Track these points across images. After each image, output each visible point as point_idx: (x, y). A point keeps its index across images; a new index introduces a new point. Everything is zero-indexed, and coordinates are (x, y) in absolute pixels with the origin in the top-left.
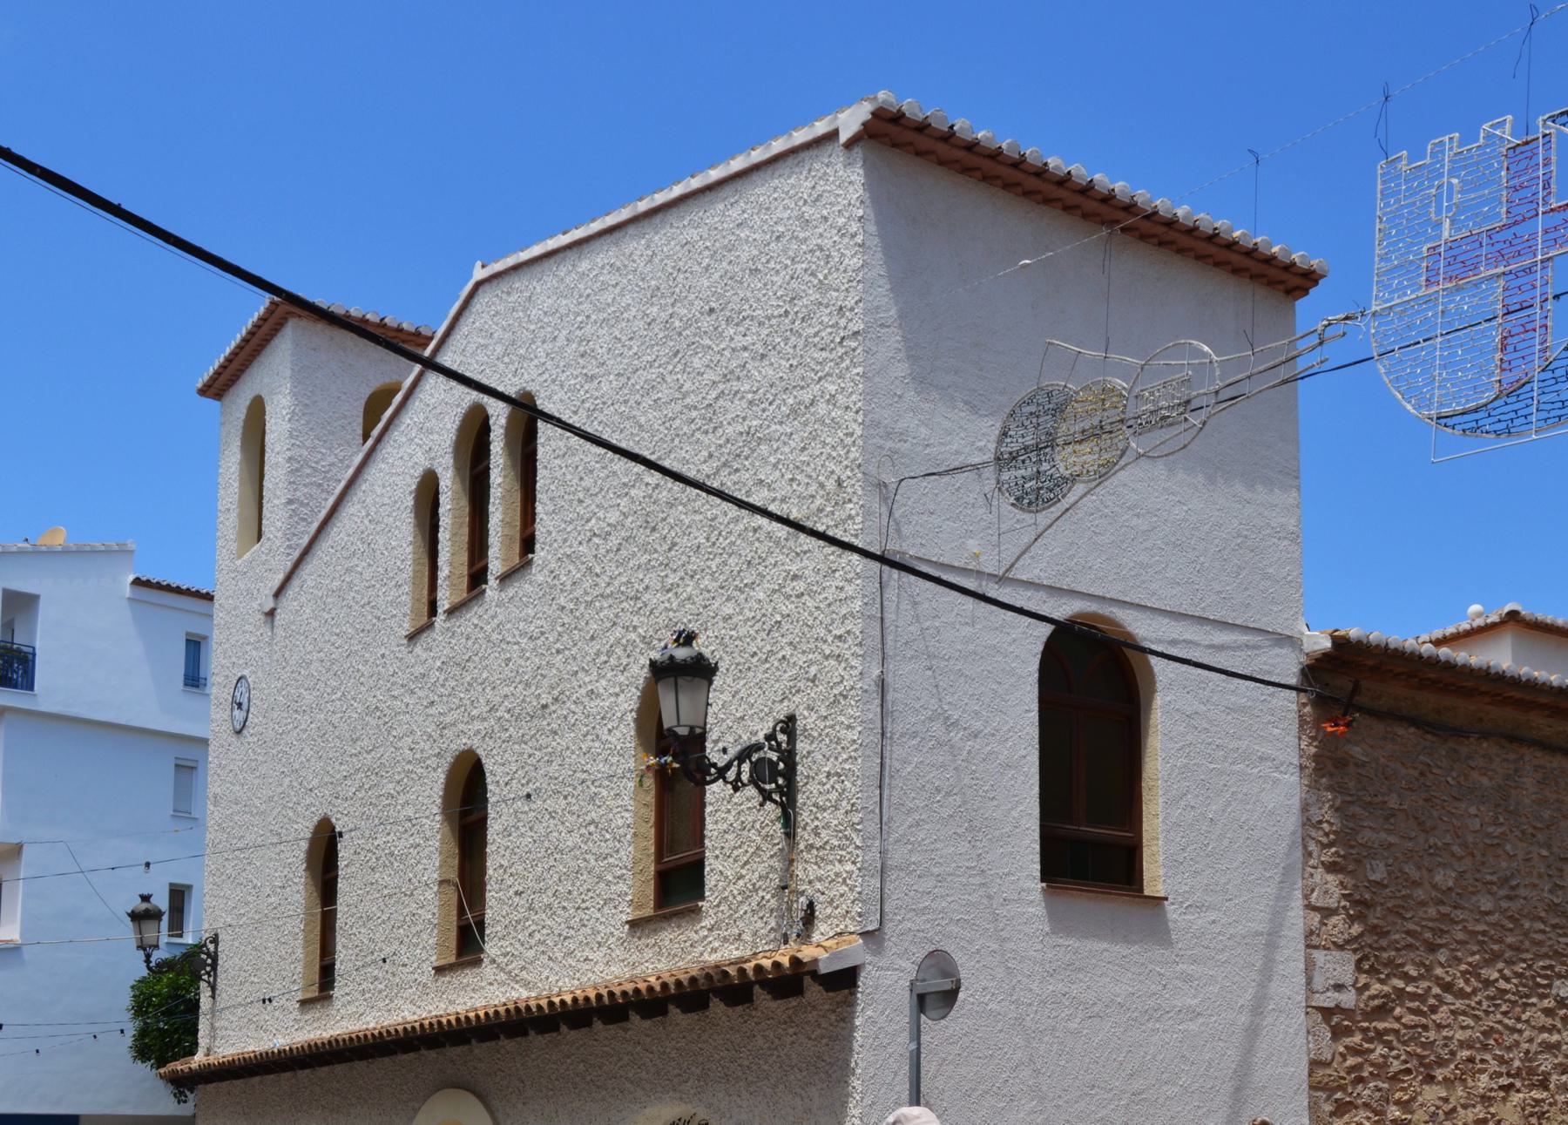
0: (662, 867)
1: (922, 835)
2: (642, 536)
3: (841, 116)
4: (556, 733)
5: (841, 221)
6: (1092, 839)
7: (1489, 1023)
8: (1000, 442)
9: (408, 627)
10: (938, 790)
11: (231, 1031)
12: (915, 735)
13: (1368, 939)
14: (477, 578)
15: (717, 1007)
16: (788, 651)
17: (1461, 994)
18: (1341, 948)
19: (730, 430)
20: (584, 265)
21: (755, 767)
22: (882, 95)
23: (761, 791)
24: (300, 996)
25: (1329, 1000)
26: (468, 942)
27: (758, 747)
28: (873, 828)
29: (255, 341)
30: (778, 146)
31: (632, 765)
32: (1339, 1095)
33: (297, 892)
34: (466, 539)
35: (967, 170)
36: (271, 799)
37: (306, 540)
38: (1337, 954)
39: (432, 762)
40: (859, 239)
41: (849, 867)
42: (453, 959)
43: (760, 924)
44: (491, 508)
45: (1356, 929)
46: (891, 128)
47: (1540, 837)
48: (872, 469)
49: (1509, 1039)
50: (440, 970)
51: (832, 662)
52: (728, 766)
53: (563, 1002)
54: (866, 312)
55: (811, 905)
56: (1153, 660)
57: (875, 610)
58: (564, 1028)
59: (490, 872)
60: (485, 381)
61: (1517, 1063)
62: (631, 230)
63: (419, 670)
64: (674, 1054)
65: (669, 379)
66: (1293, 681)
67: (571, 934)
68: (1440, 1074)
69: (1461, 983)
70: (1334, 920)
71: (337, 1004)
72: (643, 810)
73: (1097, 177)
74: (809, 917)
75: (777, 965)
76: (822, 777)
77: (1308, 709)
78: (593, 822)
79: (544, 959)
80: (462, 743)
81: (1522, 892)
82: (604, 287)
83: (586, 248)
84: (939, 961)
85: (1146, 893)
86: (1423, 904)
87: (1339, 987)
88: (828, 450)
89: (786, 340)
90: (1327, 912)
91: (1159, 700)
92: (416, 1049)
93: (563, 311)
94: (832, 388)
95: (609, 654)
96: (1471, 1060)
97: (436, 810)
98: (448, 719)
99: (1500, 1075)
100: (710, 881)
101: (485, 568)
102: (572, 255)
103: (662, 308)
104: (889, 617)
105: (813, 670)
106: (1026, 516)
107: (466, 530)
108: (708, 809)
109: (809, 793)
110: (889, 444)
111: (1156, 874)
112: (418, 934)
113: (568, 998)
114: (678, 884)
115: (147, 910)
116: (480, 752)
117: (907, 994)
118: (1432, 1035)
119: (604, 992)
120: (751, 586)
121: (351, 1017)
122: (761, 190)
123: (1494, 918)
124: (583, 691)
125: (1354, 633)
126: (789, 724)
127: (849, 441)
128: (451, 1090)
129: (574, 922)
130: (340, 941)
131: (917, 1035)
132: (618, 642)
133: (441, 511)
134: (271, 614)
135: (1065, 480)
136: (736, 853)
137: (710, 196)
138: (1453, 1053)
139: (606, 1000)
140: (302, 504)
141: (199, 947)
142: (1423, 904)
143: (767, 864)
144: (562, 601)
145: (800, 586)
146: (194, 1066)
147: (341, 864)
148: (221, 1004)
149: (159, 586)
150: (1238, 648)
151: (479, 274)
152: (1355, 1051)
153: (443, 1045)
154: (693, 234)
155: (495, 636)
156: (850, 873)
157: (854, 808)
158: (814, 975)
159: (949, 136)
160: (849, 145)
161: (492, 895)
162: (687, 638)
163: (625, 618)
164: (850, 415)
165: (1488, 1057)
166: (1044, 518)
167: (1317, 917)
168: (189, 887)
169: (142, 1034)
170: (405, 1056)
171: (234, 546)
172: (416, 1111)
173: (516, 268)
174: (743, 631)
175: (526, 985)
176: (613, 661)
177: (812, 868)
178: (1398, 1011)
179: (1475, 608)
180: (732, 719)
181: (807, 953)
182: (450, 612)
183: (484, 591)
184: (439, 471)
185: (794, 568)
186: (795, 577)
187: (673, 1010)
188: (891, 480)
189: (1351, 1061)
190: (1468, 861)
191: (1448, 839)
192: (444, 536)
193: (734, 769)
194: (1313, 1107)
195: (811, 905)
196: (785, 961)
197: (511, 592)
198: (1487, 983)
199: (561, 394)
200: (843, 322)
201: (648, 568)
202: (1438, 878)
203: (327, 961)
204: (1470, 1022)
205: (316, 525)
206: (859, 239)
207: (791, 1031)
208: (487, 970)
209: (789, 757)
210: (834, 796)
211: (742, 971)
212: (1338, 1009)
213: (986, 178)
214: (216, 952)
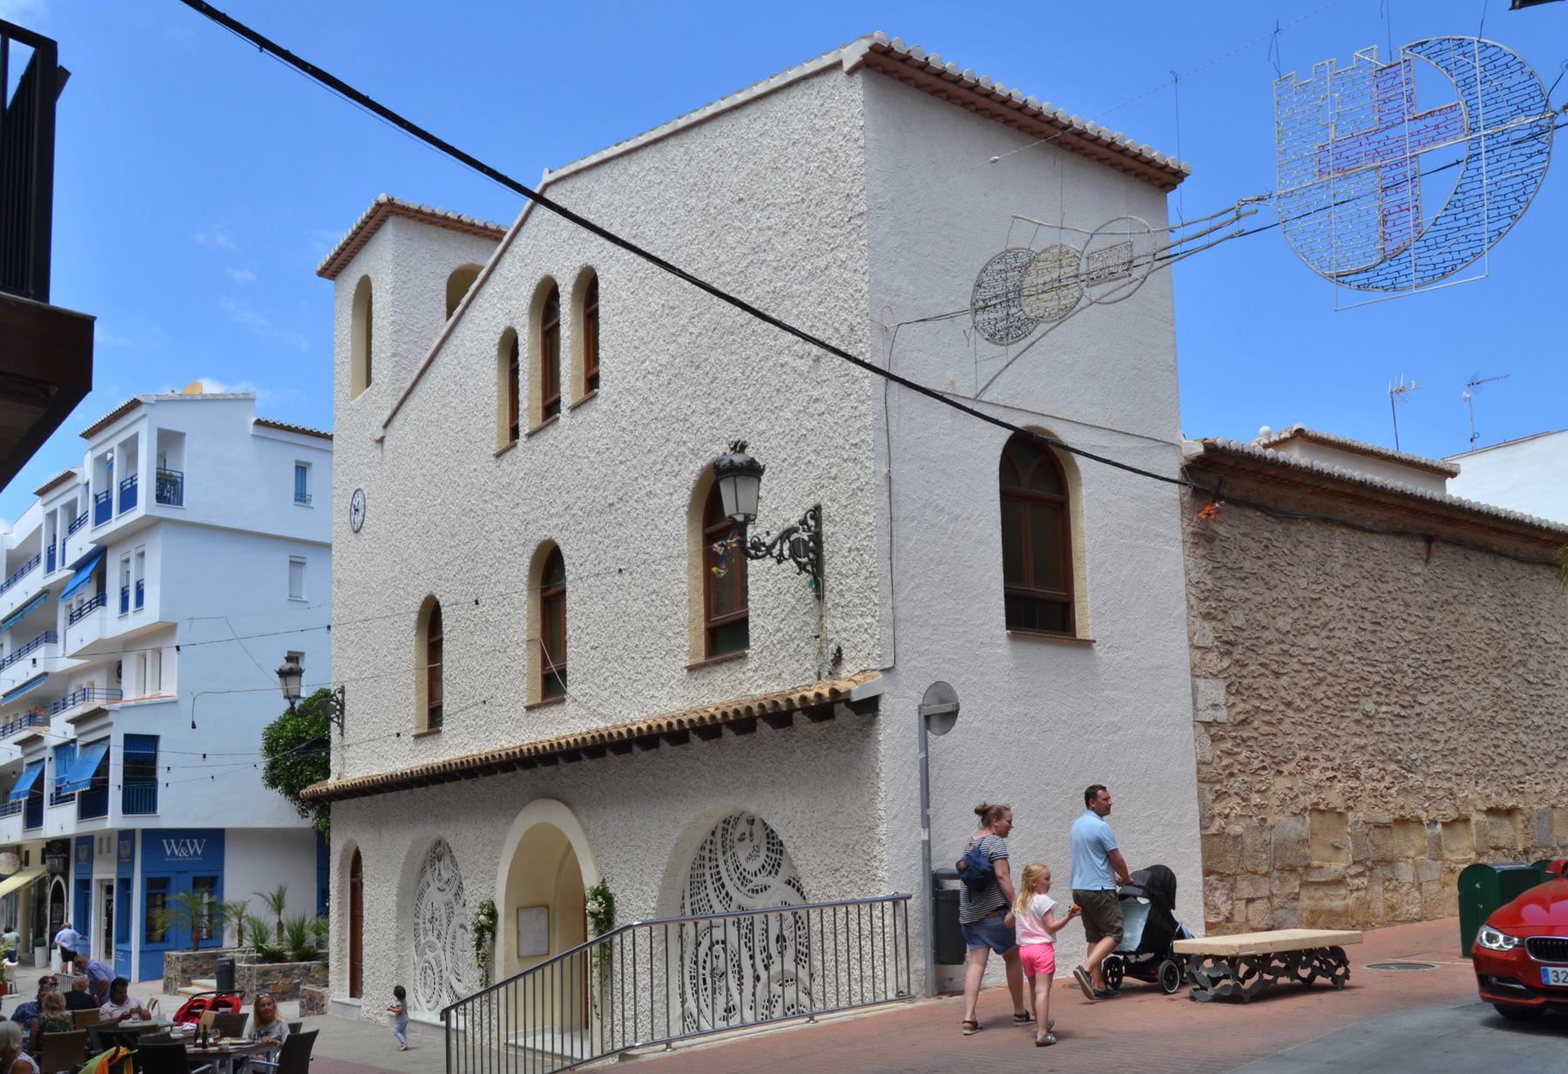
1: (921, 595)
2: (688, 372)
3: (844, 51)
5: (846, 129)
6: (1040, 601)
7: (1318, 730)
8: (975, 291)
10: (931, 560)
11: (356, 759)
12: (913, 519)
13: (1234, 670)
14: (551, 409)
16: (813, 457)
17: (1299, 710)
19: (758, 290)
21: (793, 544)
22: (877, 34)
23: (799, 563)
24: (415, 732)
25: (1207, 716)
26: (552, 686)
27: (794, 530)
28: (887, 590)
29: (363, 233)
30: (792, 75)
31: (685, 547)
32: (1218, 787)
33: (410, 651)
34: (540, 379)
35: (935, 92)
36: (385, 582)
37: (408, 385)
38: (1213, 682)
39: (519, 550)
40: (861, 143)
41: (869, 620)
43: (796, 665)
44: (562, 355)
45: (1226, 662)
46: (883, 59)
48: (877, 317)
49: (1333, 742)
50: (530, 708)
51: (850, 464)
52: (773, 545)
53: (639, 729)
54: (868, 198)
55: (839, 650)
57: (882, 424)
58: (561, 762)
59: (569, 632)
61: (1338, 761)
62: (672, 141)
63: (505, 480)
65: (707, 253)
66: (1176, 477)
68: (1286, 768)
70: (1211, 656)
71: (445, 737)
73: (1030, 98)
74: (838, 658)
75: (818, 695)
76: (845, 552)
77: (1186, 499)
78: (654, 592)
79: (617, 697)
80: (543, 535)
81: (1337, 633)
82: (651, 184)
83: (635, 156)
84: (941, 691)
85: (1079, 636)
86: (1270, 643)
87: (1215, 706)
88: (841, 303)
89: (804, 220)
90: (1207, 650)
92: (442, 782)
93: (617, 204)
94: (843, 256)
95: (664, 463)
96: (1306, 759)
97: (523, 587)
99: (1326, 769)
100: (754, 633)
101: (558, 401)
102: (624, 162)
103: (700, 199)
104: (893, 429)
105: (834, 471)
106: (998, 348)
107: (540, 373)
108: (750, 579)
109: (834, 564)
110: (888, 298)
111: (1087, 620)
112: (511, 682)
113: (644, 727)
114: (726, 635)
116: (559, 541)
117: (916, 716)
118: (1280, 740)
119: (674, 721)
120: (780, 408)
121: (459, 744)
122: (777, 105)
123: (1317, 653)
124: (643, 492)
125: (1220, 442)
127: (858, 295)
128: (540, 801)
129: (642, 668)
130: (447, 689)
131: (925, 746)
132: (671, 453)
133: (520, 358)
134: (381, 441)
135: (1031, 321)
137: (736, 114)
138: (1294, 754)
139: (675, 726)
141: (324, 696)
142: (1270, 643)
144: (623, 424)
145: (821, 407)
146: (331, 787)
147: (445, 630)
149: (275, 426)
152: (1229, 754)
153: (476, 776)
154: (723, 142)
155: (568, 453)
156: (870, 624)
157: (871, 575)
158: (848, 702)
159: (924, 66)
160: (851, 72)
161: (572, 650)
162: (740, 447)
163: (676, 436)
164: (858, 276)
165: (1318, 756)
166: (1014, 349)
167: (1198, 654)
169: (272, 766)
170: (504, 775)
171: (348, 391)
172: (514, 817)
173: (577, 173)
174: (775, 443)
176: (667, 469)
177: (839, 623)
178: (1256, 724)
179: (1264, 429)
180: (773, 509)
181: (842, 686)
182: (530, 435)
184: (517, 328)
185: (815, 394)
186: (817, 400)
187: (636, 749)
188: (891, 325)
189: (1225, 762)
190: (1300, 610)
191: (1285, 594)
192: (523, 377)
194: (1201, 796)
195: (839, 650)
196: (826, 692)
197: (580, 418)
198: (1315, 701)
199: (618, 267)
200: (850, 206)
201: (694, 397)
203: (435, 704)
204: (1304, 730)
205: (417, 372)
206: (861, 143)
208: (569, 706)
209: (817, 537)
210: (855, 566)
211: (790, 701)
212: (1215, 723)
213: (950, 99)
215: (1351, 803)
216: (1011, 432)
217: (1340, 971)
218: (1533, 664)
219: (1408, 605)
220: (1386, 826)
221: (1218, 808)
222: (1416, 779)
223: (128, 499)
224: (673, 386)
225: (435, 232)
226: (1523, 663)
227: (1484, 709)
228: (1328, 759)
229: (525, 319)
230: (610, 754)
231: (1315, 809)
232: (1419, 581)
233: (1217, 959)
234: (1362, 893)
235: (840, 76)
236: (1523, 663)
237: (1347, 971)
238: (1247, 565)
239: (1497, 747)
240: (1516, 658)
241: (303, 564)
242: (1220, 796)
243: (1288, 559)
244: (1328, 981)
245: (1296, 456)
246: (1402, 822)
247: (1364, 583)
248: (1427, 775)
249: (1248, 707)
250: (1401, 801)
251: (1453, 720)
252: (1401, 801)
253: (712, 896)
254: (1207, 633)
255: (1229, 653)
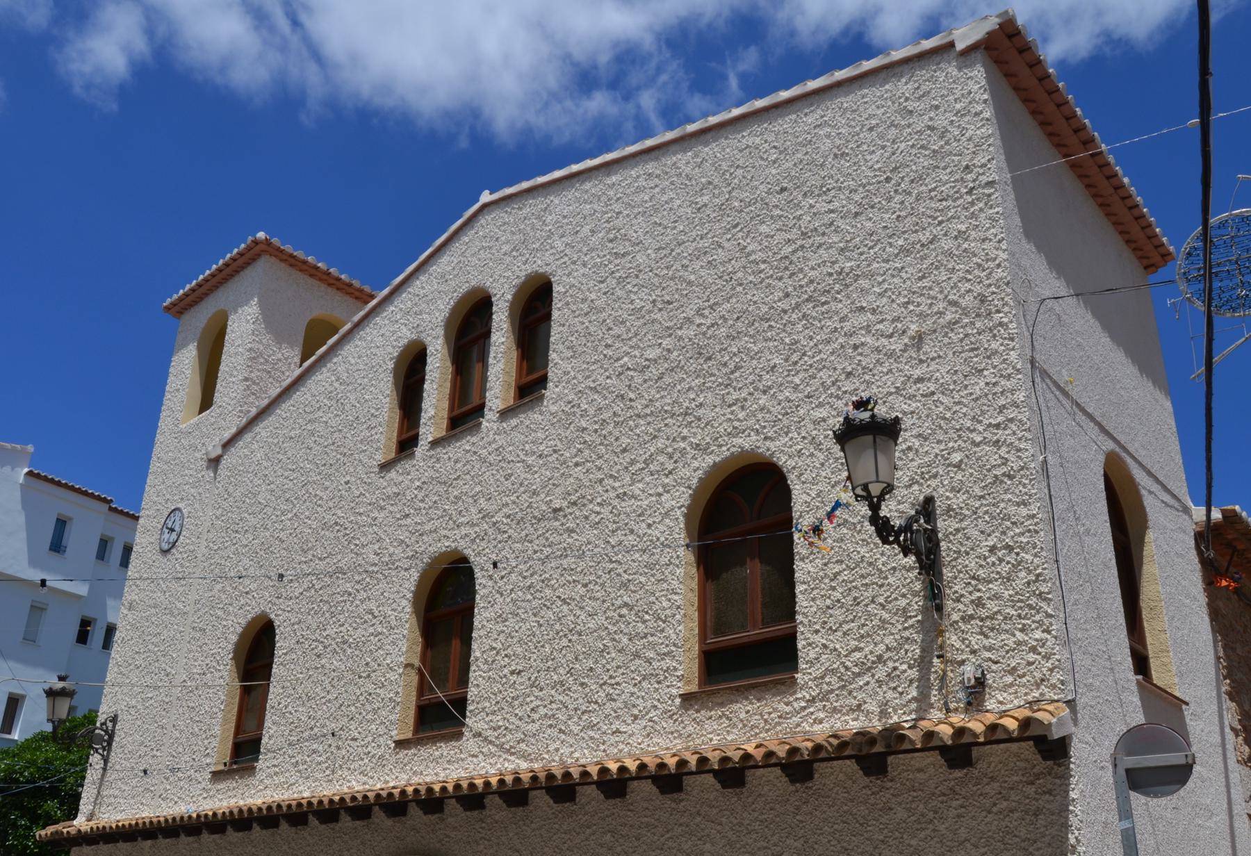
0: (706, 648)
4: (573, 531)
9: (380, 457)
14: (465, 415)
15: (345, 820)
20: (614, 179)
24: (213, 769)
33: (223, 679)
42: (409, 735)
50: (400, 744)
64: (756, 826)
71: (260, 775)
72: (690, 595)
79: (555, 732)
91: (1150, 536)
98: (427, 527)
108: (799, 588)
115: (63, 689)
131: (1125, 812)
134: (215, 462)
136: (846, 627)
140: (254, 383)
143: (899, 635)
148: (111, 776)
150: (1171, 507)
151: (486, 197)
156: (1043, 643)
168: (23, 697)
175: (525, 756)
183: (480, 424)
184: (428, 340)
187: (229, 829)
201: (702, 389)
207: (955, 804)
208: (469, 742)
214: (113, 731)
224: (667, 379)
225: (302, 278)
230: (284, 826)
241: (43, 609)
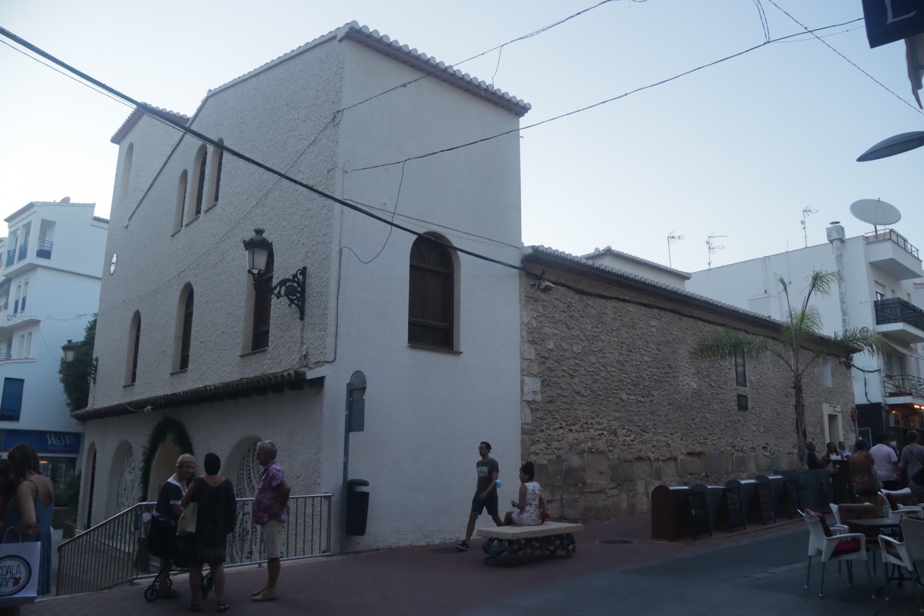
11: (99, 399)
17: (583, 396)
18: (535, 376)
27: (288, 280)
45: (543, 368)
47: (614, 333)
56: (459, 253)
60: (241, 153)
67: (220, 360)
69: (583, 392)
80: (186, 281)
100: (271, 338)
114: (259, 340)
121: (141, 392)
123: (595, 366)
126: (304, 271)
134: (127, 227)
160: (340, 41)
162: (259, 232)
167: (526, 363)
178: (558, 403)
182: (187, 226)
193: (278, 289)
198: (593, 392)
202: (575, 349)
204: (587, 408)
209: (303, 286)
215: (611, 448)
216: (416, 236)
217: (571, 547)
218: (714, 377)
219: (647, 342)
220: (630, 461)
221: (533, 448)
222: (647, 436)
223: (23, 255)
226: (709, 376)
227: (687, 399)
228: (599, 424)
229: (192, 165)
231: (590, 451)
232: (654, 330)
233: (500, 541)
234: (615, 498)
235: (336, 42)
236: (709, 376)
237: (574, 547)
238: (557, 316)
239: (693, 419)
240: (705, 373)
242: (534, 443)
243: (581, 313)
244: (564, 553)
245: (608, 264)
246: (640, 459)
247: (623, 329)
248: (656, 434)
249: (554, 394)
250: (640, 447)
251: (670, 404)
252: (640, 447)
253: (246, 487)
254: (531, 353)
255: (544, 363)
